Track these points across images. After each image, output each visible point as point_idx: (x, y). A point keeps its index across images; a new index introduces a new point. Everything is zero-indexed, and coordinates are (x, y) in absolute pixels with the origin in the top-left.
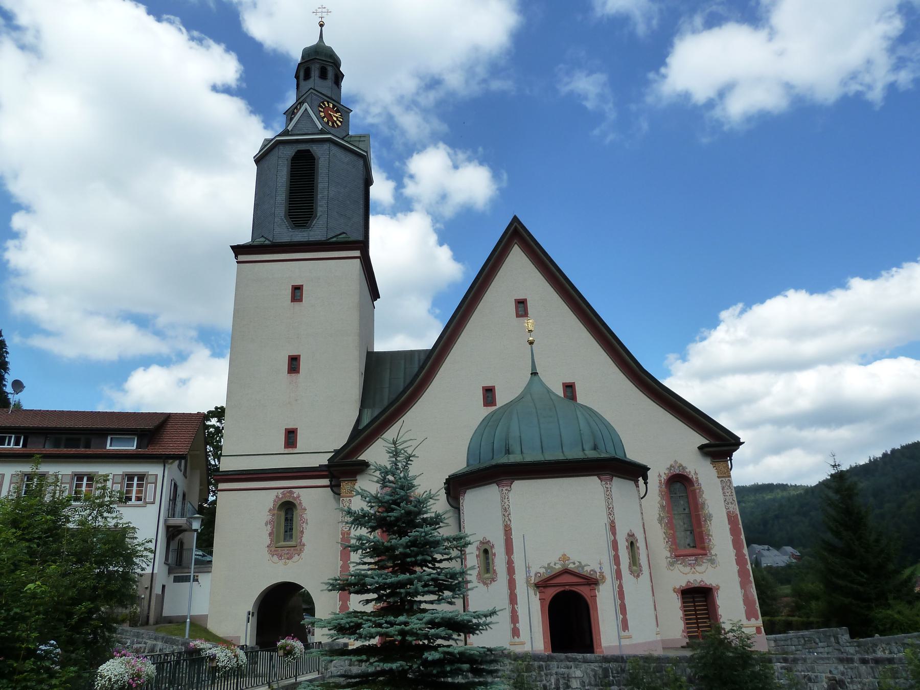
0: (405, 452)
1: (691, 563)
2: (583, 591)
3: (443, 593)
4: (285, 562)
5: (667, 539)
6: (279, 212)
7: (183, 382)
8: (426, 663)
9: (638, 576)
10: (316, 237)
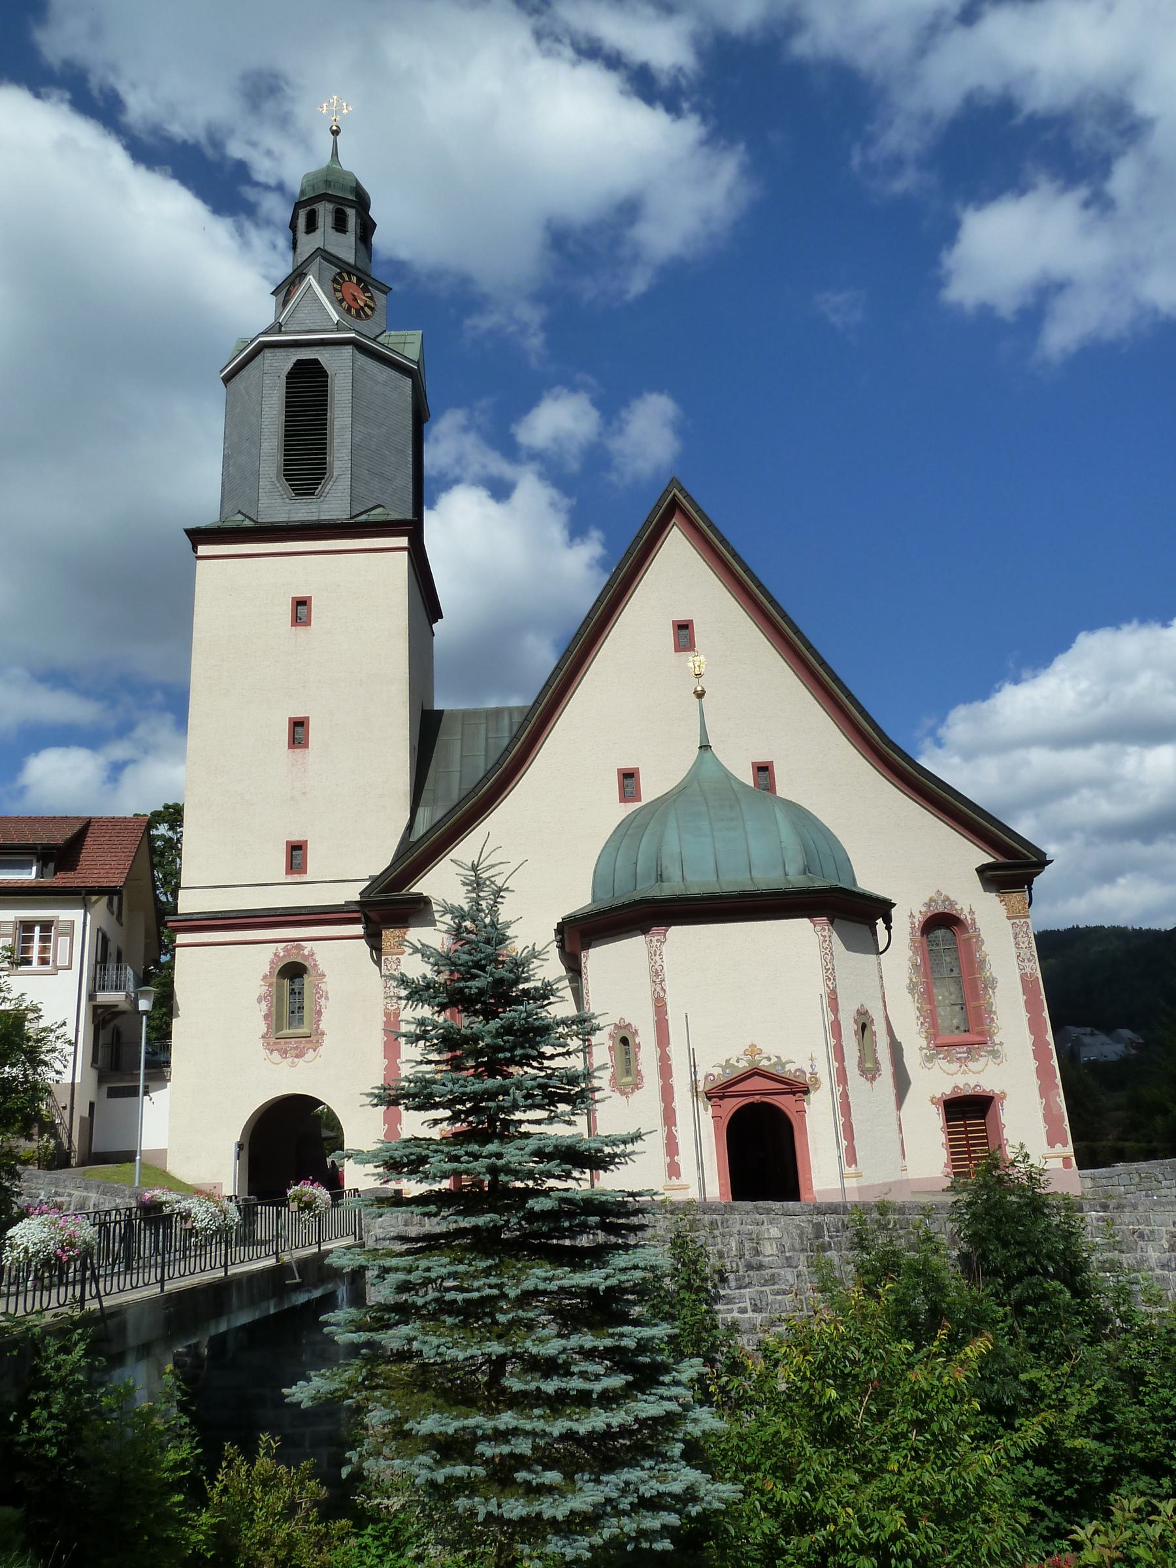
0: (493, 883)
2: (784, 1103)
3: (557, 1107)
4: (293, 1063)
5: (922, 1019)
7: (116, 770)
8: (532, 1216)
9: (873, 1079)
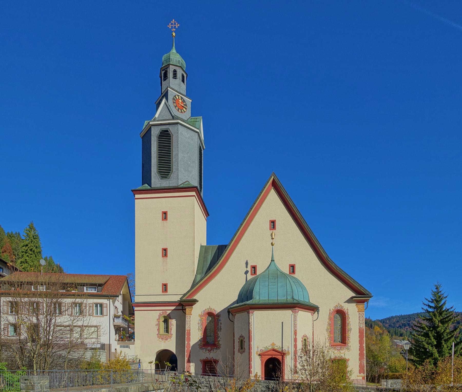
1: (338, 349)
5: (329, 338)
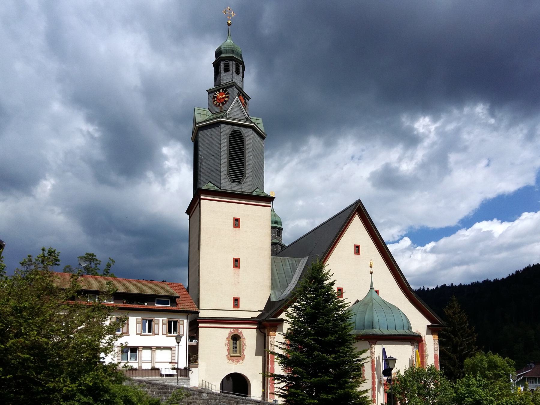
6: (224, 170)
10: (245, 190)
